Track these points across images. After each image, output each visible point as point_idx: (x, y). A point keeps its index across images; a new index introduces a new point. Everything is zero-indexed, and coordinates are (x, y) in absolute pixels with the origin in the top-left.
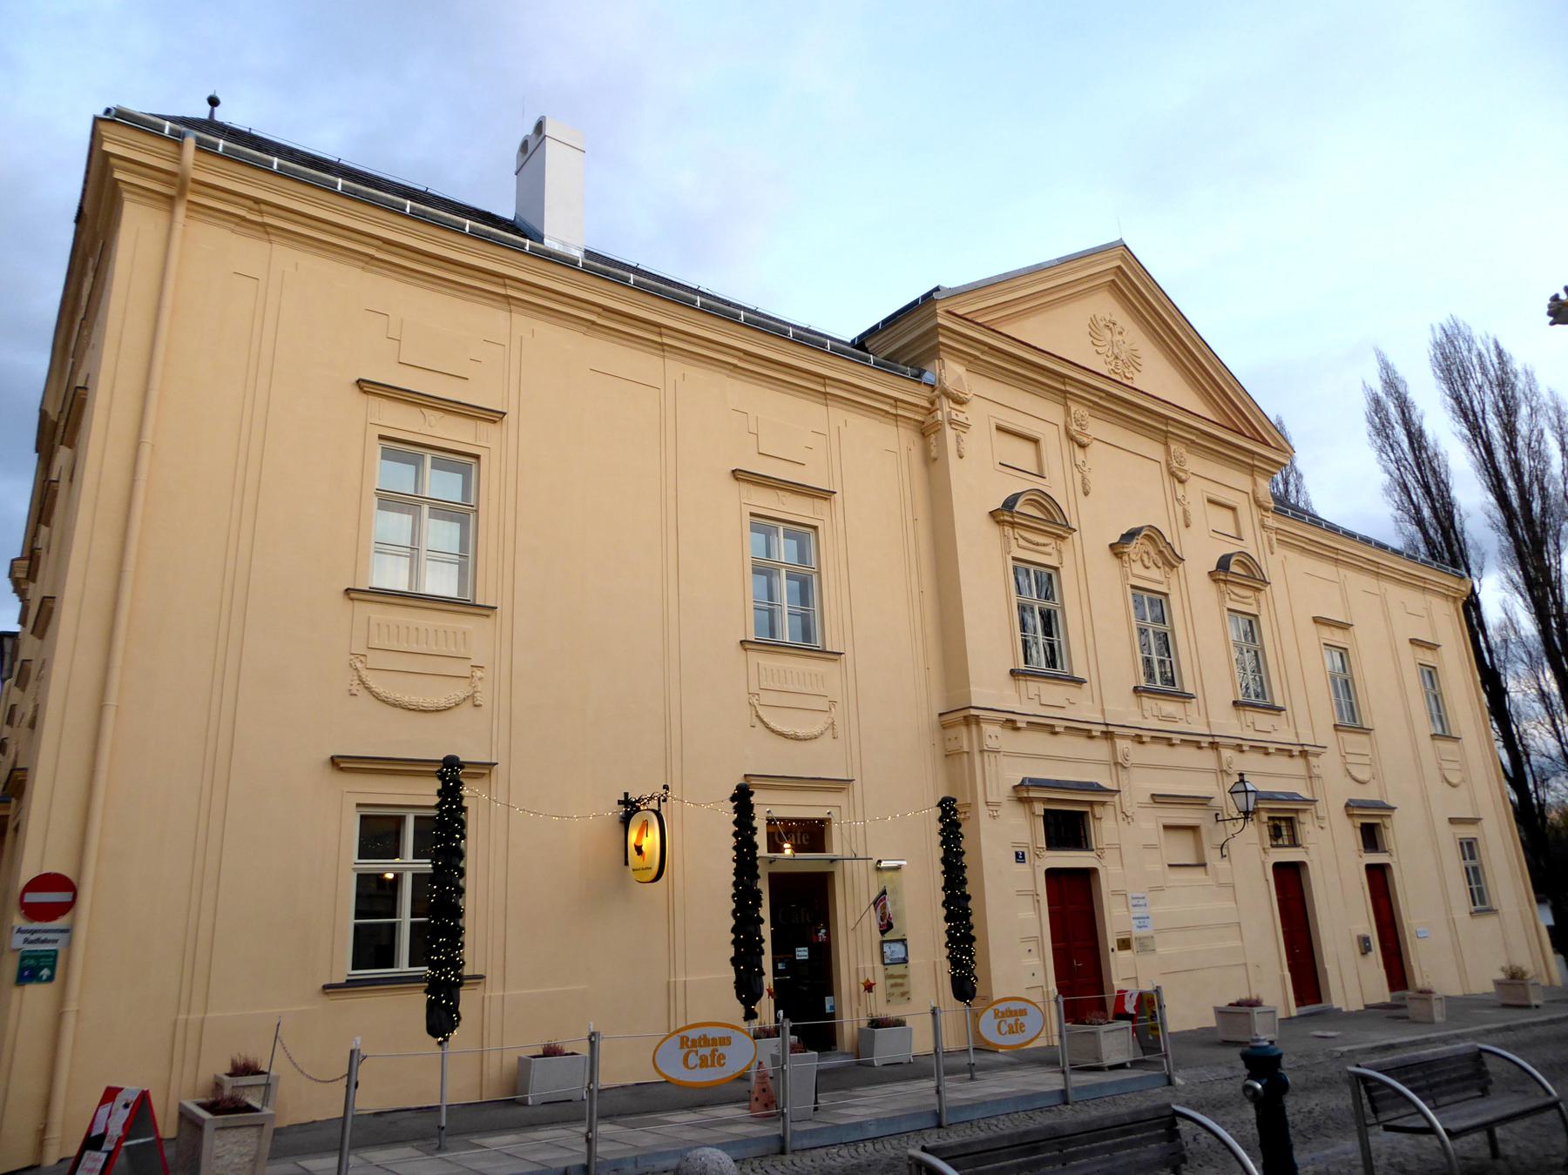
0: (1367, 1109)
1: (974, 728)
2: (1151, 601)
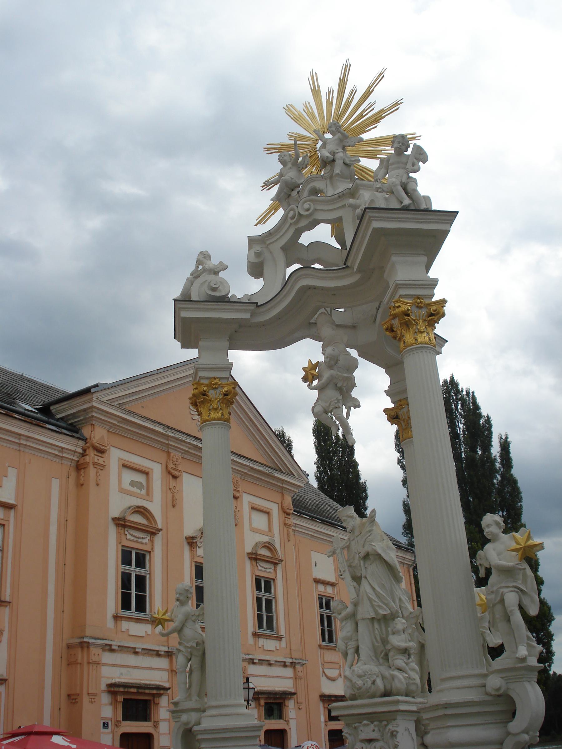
1: (86, 649)
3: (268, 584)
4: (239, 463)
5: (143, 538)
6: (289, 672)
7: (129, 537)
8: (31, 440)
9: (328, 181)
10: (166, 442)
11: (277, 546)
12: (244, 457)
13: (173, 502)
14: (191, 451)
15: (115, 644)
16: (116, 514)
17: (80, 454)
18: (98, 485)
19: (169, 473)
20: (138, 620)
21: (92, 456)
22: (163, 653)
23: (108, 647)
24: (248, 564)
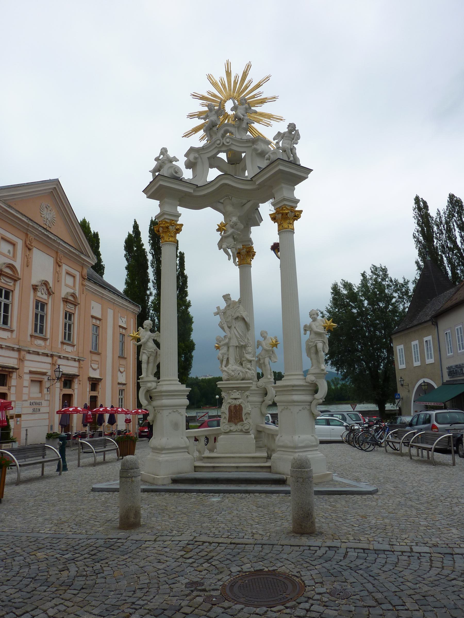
3: (70, 316)
6: (76, 364)
9: (236, 129)
11: (77, 295)
12: (67, 243)
13: (27, 264)
19: (27, 246)
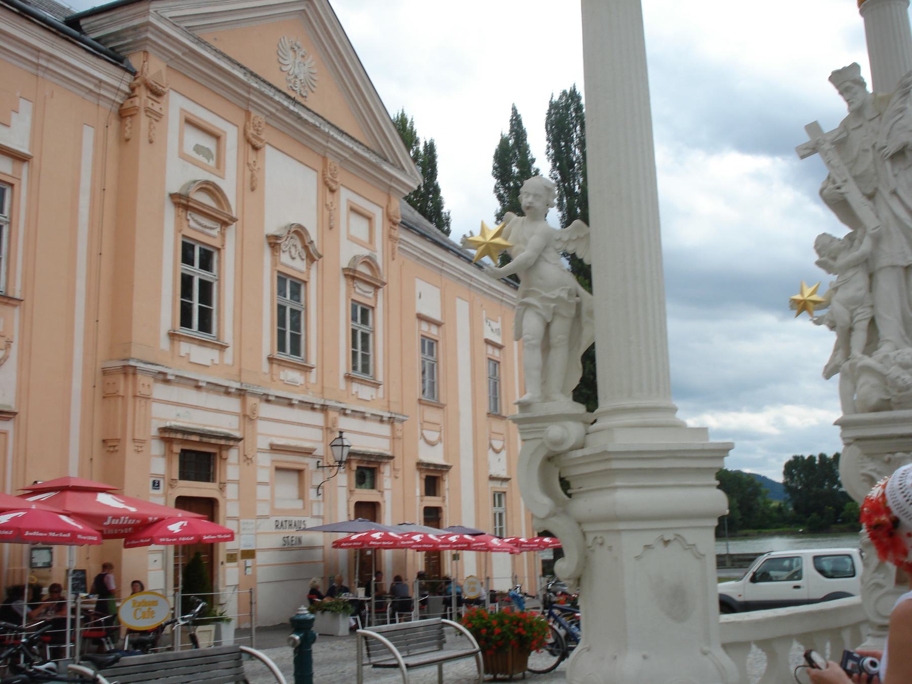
0: (365, 652)
1: (130, 377)
2: (429, 343)
3: (365, 312)
4: (339, 142)
5: (211, 228)
6: (385, 430)
7: (192, 223)
8: (54, 60)
10: (246, 95)
11: (379, 261)
12: (346, 134)
13: (252, 183)
14: (278, 114)
15: (171, 373)
16: (175, 189)
17: (127, 94)
18: (151, 142)
20: (203, 343)
21: (143, 98)
22: (233, 390)
23: (161, 377)
24: (343, 283)
